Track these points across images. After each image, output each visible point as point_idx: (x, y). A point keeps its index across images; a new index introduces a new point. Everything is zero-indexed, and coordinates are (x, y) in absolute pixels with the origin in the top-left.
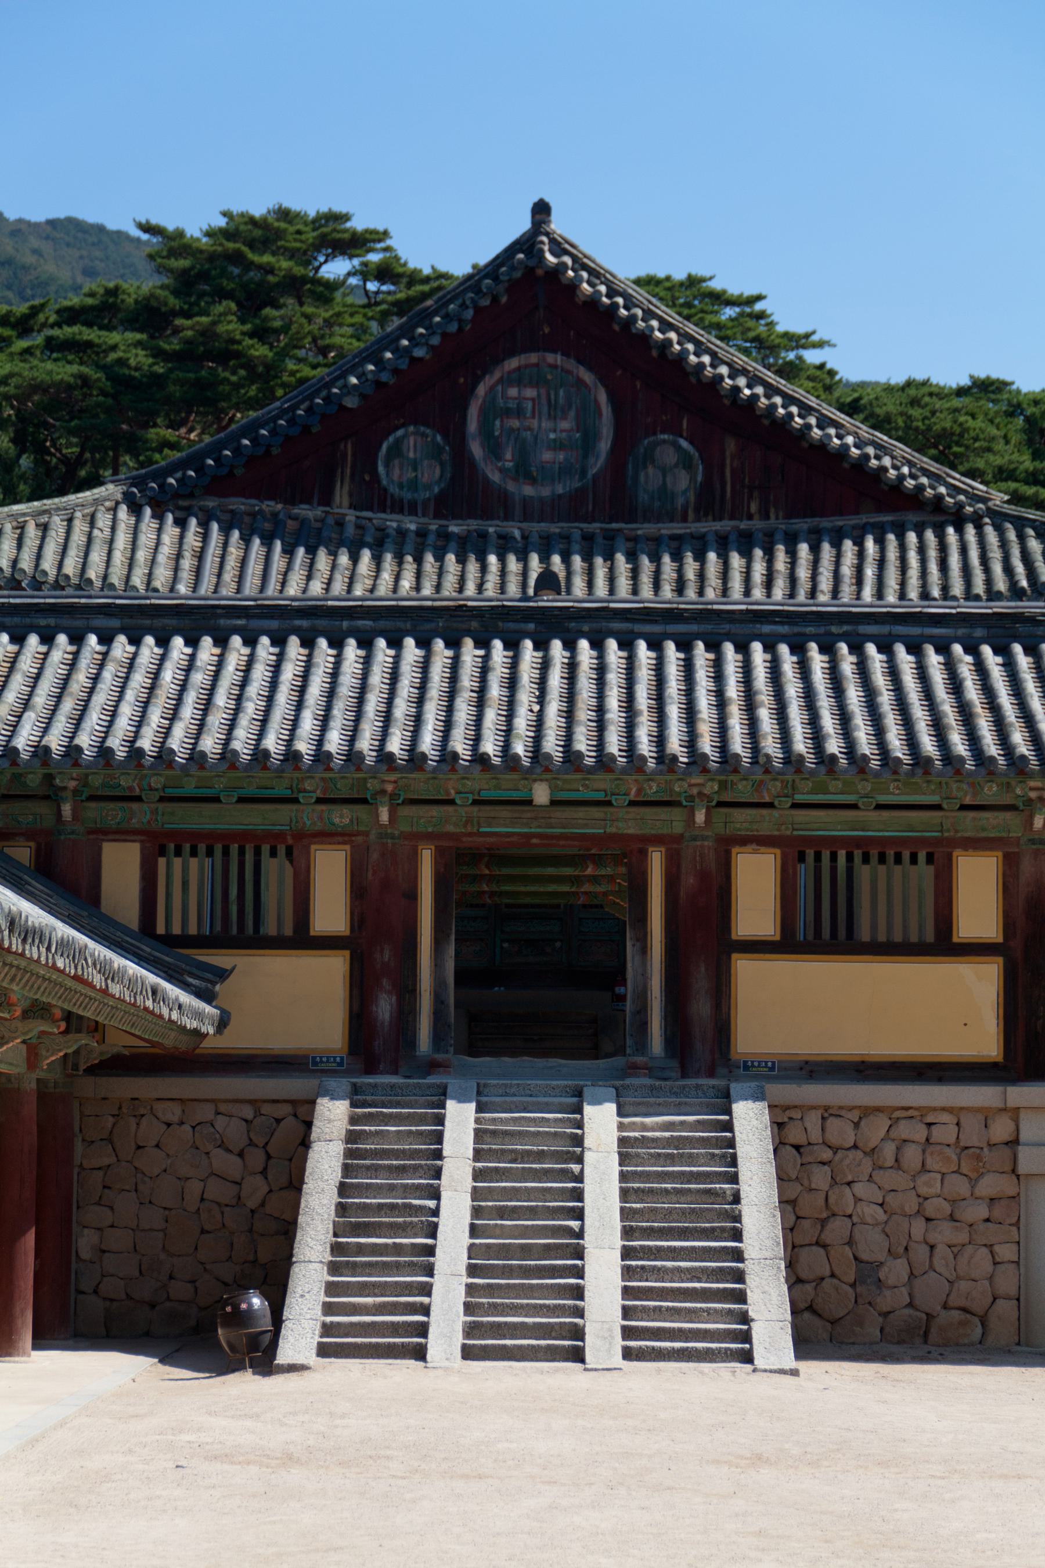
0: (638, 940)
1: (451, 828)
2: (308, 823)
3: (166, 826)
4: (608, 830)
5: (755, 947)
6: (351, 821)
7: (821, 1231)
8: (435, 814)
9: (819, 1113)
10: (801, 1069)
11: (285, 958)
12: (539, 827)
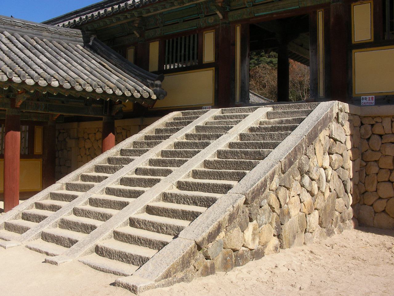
0: (313, 50)
1: (245, 17)
2: (202, 24)
3: (164, 34)
4: (301, 6)
5: (363, 46)
6: (214, 20)
7: (390, 175)
8: (240, 12)
9: (389, 119)
10: (384, 99)
11: (198, 73)
12: (275, 10)
